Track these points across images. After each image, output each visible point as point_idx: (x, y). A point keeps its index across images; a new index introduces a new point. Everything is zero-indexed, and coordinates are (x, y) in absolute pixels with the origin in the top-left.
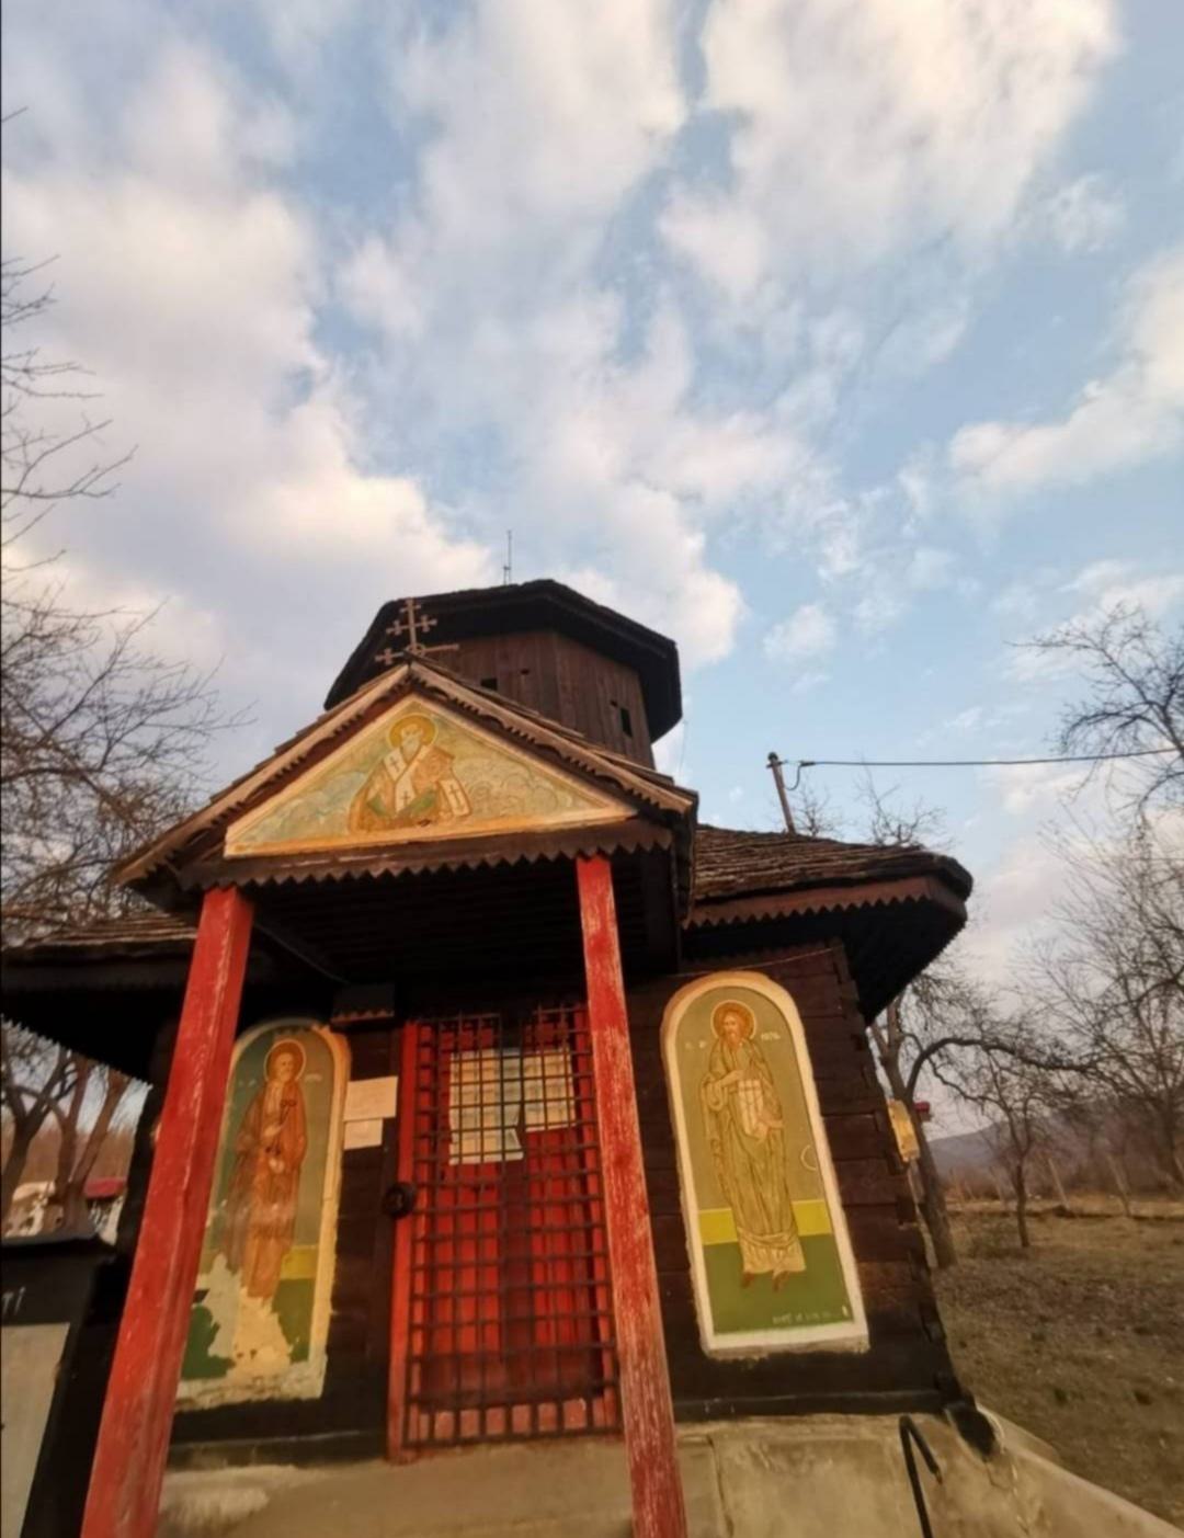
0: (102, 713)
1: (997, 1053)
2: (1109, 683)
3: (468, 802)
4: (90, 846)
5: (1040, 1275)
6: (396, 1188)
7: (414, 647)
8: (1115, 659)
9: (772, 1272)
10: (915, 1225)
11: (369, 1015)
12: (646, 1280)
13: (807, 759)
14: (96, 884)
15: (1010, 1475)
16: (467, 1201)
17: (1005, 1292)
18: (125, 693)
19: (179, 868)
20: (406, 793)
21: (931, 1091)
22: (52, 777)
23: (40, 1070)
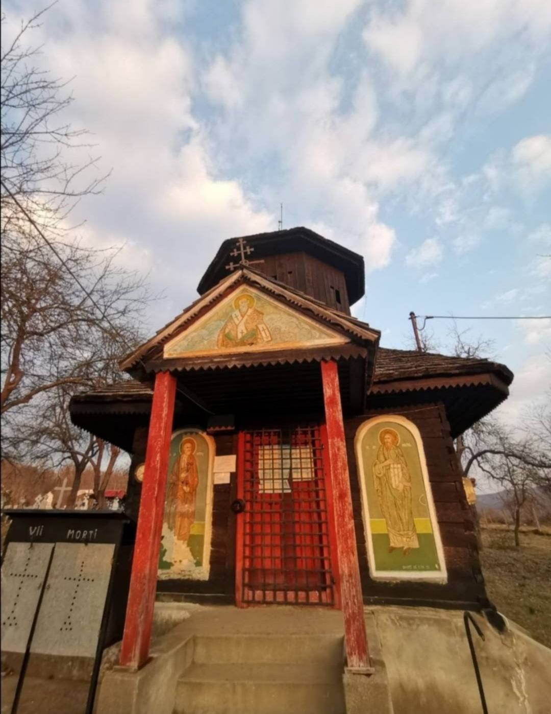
0: (101, 294)
1: (512, 459)
3: (271, 335)
4: (99, 353)
5: (525, 559)
6: (237, 502)
7: (243, 262)
9: (403, 547)
10: (472, 532)
11: (223, 428)
12: (352, 547)
14: (103, 369)
15: (512, 641)
16: (266, 509)
17: (506, 565)
18: (111, 285)
19: (145, 363)
21: (476, 474)
22: (83, 323)
23: (83, 445)
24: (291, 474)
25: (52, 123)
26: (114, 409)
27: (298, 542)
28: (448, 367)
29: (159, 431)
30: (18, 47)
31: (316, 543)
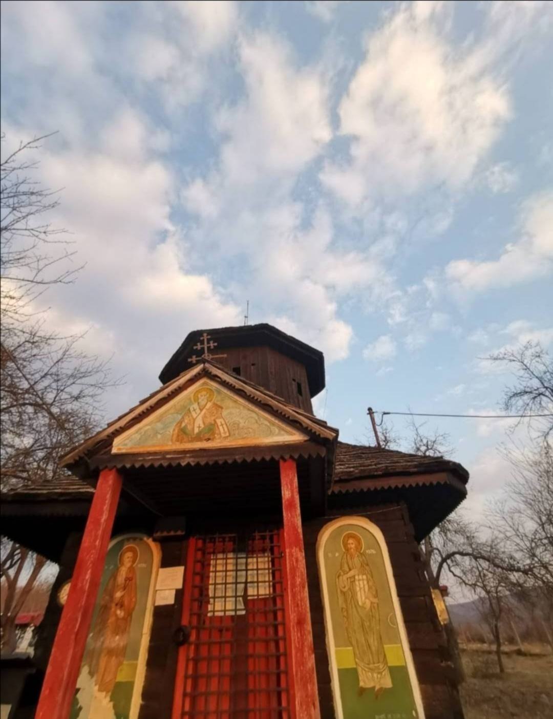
0: (56, 378)
1: (481, 561)
2: (526, 378)
3: (229, 431)
4: (42, 440)
6: (180, 629)
8: (528, 367)
9: (374, 688)
11: (172, 533)
12: (313, 695)
13: (386, 411)
14: (43, 459)
16: (215, 638)
17: (492, 699)
20: (199, 425)
24: (246, 590)
25: (32, 222)
26: (46, 511)
27: (251, 687)
28: (406, 465)
29: (95, 541)
30: (13, 161)
31: (273, 685)
